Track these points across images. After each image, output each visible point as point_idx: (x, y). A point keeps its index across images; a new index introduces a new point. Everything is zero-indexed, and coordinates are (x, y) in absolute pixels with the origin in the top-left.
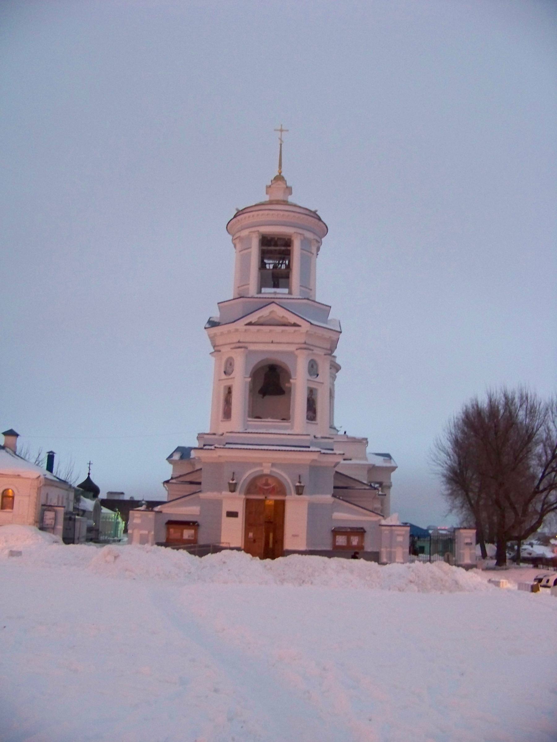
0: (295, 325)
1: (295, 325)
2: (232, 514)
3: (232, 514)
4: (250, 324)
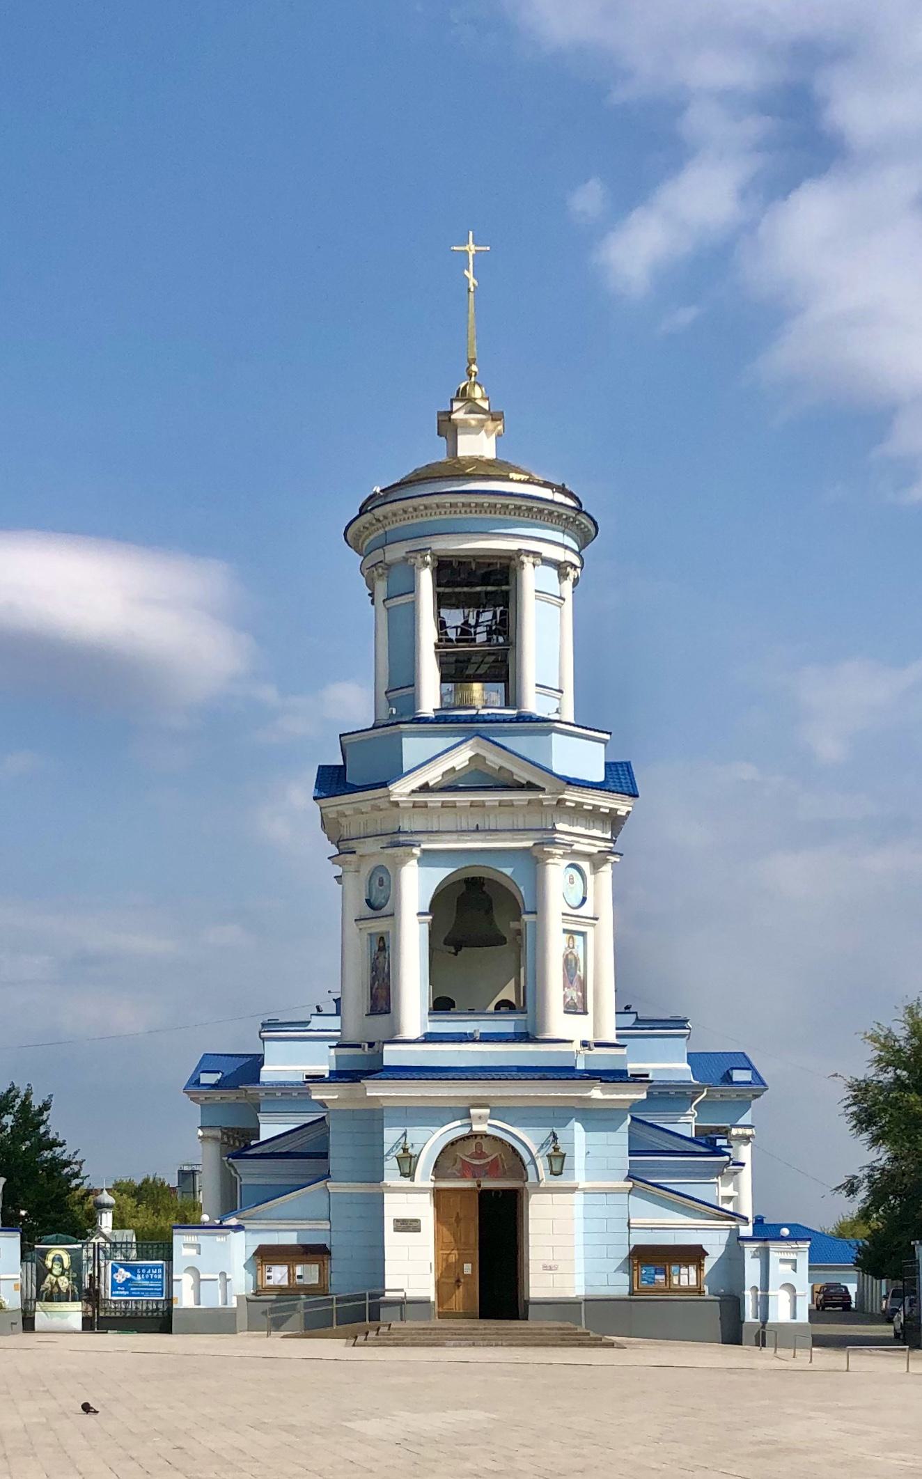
0: (530, 786)
1: (530, 786)
2: (408, 1225)
3: (408, 1225)
4: (425, 788)
